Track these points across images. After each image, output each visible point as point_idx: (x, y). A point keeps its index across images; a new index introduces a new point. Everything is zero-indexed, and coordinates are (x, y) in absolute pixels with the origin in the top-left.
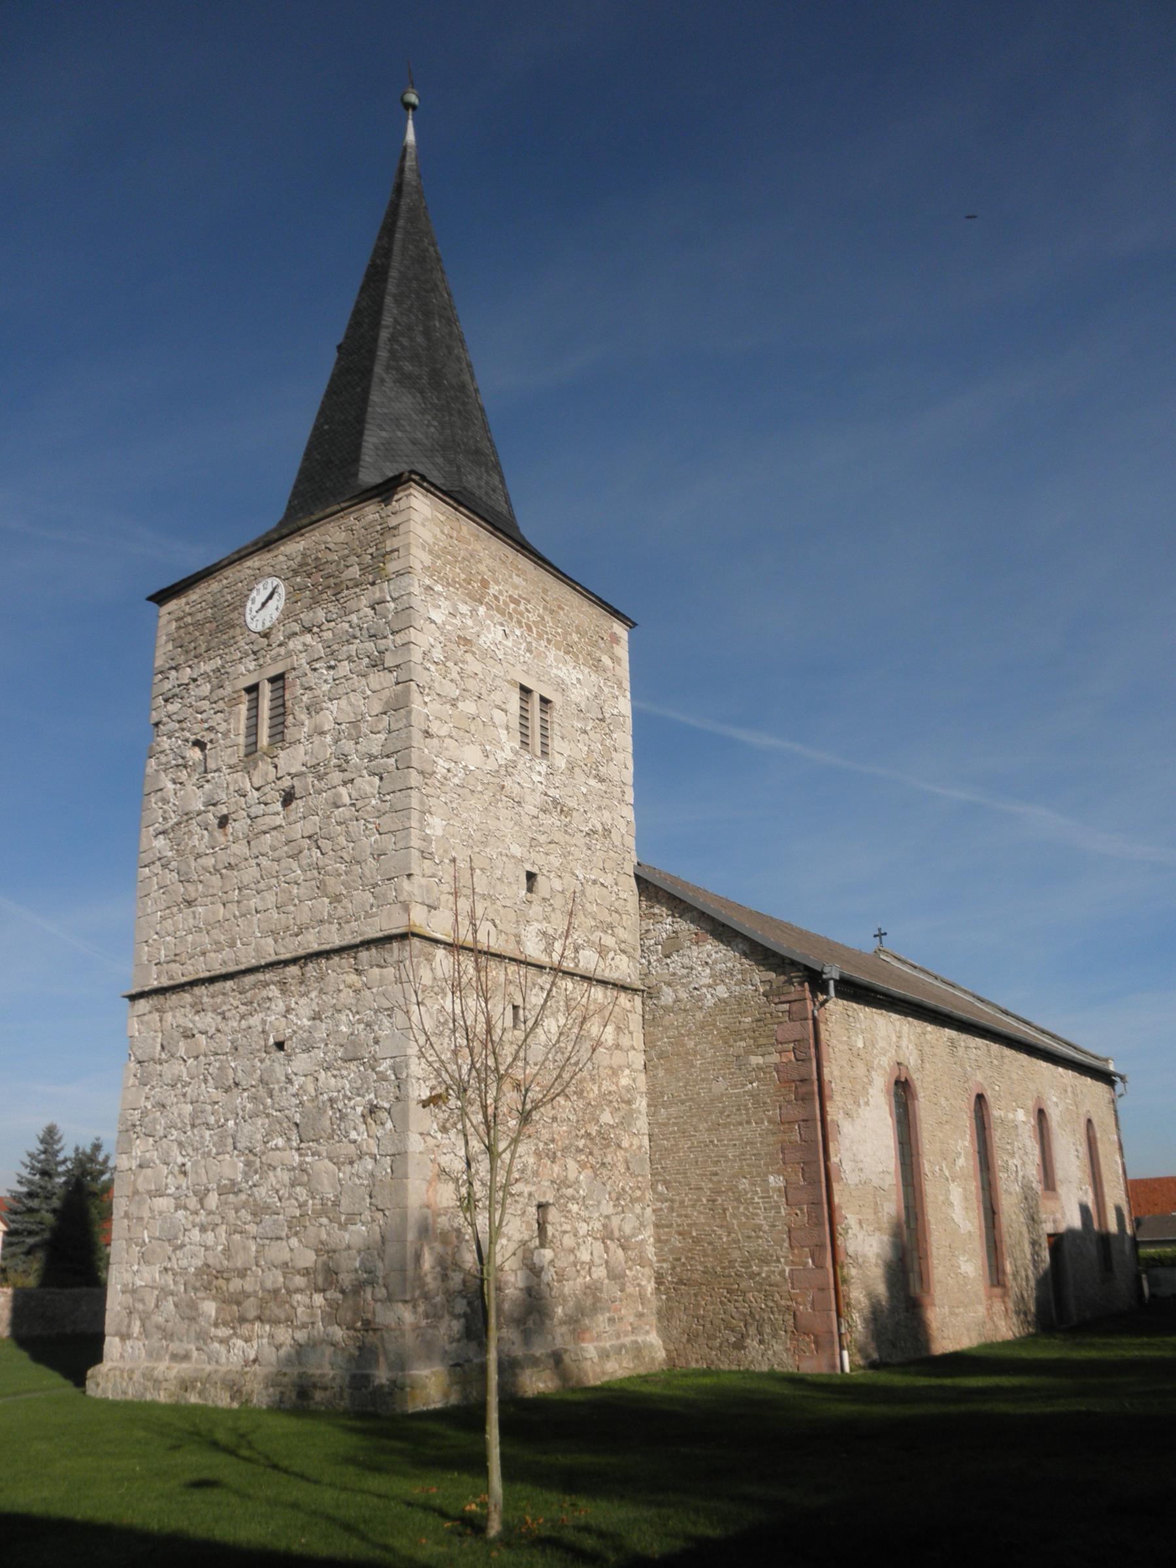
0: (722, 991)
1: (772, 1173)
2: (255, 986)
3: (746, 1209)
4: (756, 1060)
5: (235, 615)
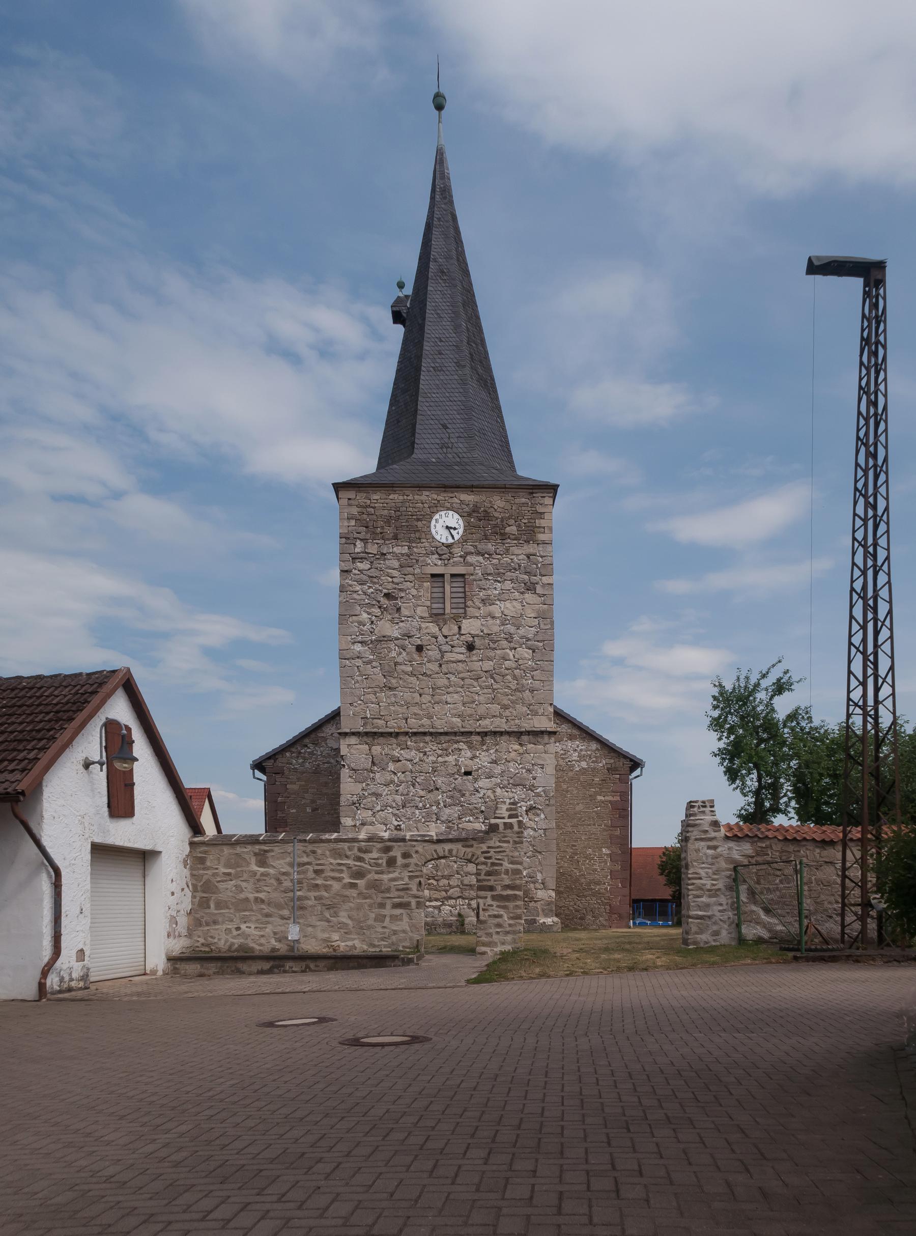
0: (584, 764)
1: (604, 848)
2: (449, 741)
3: (590, 861)
4: (599, 798)
5: (419, 524)
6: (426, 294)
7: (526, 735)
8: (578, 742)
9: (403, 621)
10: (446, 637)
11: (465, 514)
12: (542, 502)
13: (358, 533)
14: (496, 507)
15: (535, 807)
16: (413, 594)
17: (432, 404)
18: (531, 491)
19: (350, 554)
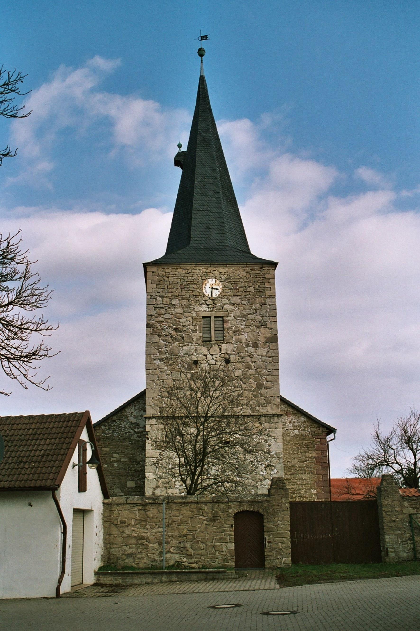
0: (296, 432)
1: (312, 489)
6: (195, 153)
7: (263, 417)
8: (292, 417)
9: (185, 346)
10: (212, 355)
11: (223, 281)
12: (268, 272)
13: (158, 292)
14: (241, 276)
15: (270, 465)
16: (192, 329)
17: (200, 214)
18: (262, 266)
19: (153, 305)
